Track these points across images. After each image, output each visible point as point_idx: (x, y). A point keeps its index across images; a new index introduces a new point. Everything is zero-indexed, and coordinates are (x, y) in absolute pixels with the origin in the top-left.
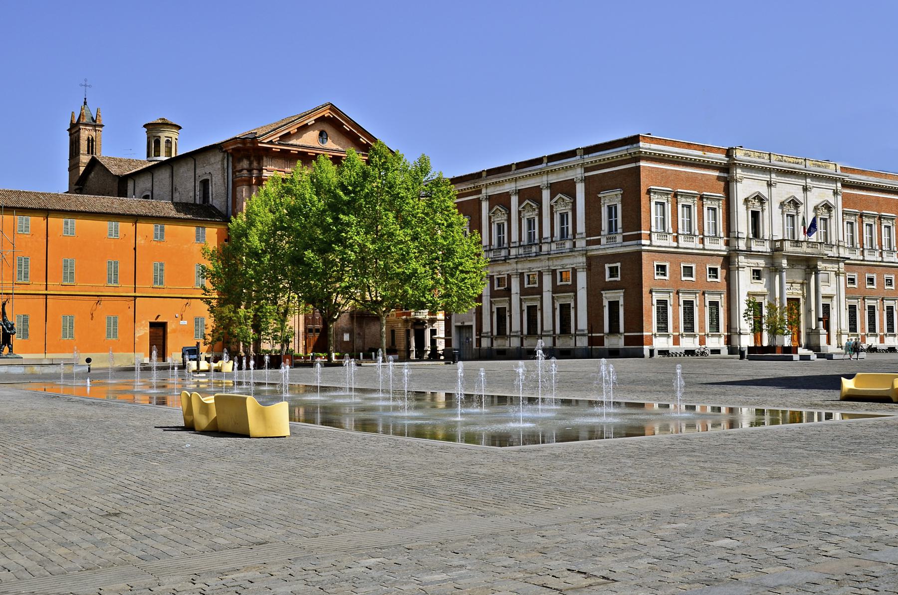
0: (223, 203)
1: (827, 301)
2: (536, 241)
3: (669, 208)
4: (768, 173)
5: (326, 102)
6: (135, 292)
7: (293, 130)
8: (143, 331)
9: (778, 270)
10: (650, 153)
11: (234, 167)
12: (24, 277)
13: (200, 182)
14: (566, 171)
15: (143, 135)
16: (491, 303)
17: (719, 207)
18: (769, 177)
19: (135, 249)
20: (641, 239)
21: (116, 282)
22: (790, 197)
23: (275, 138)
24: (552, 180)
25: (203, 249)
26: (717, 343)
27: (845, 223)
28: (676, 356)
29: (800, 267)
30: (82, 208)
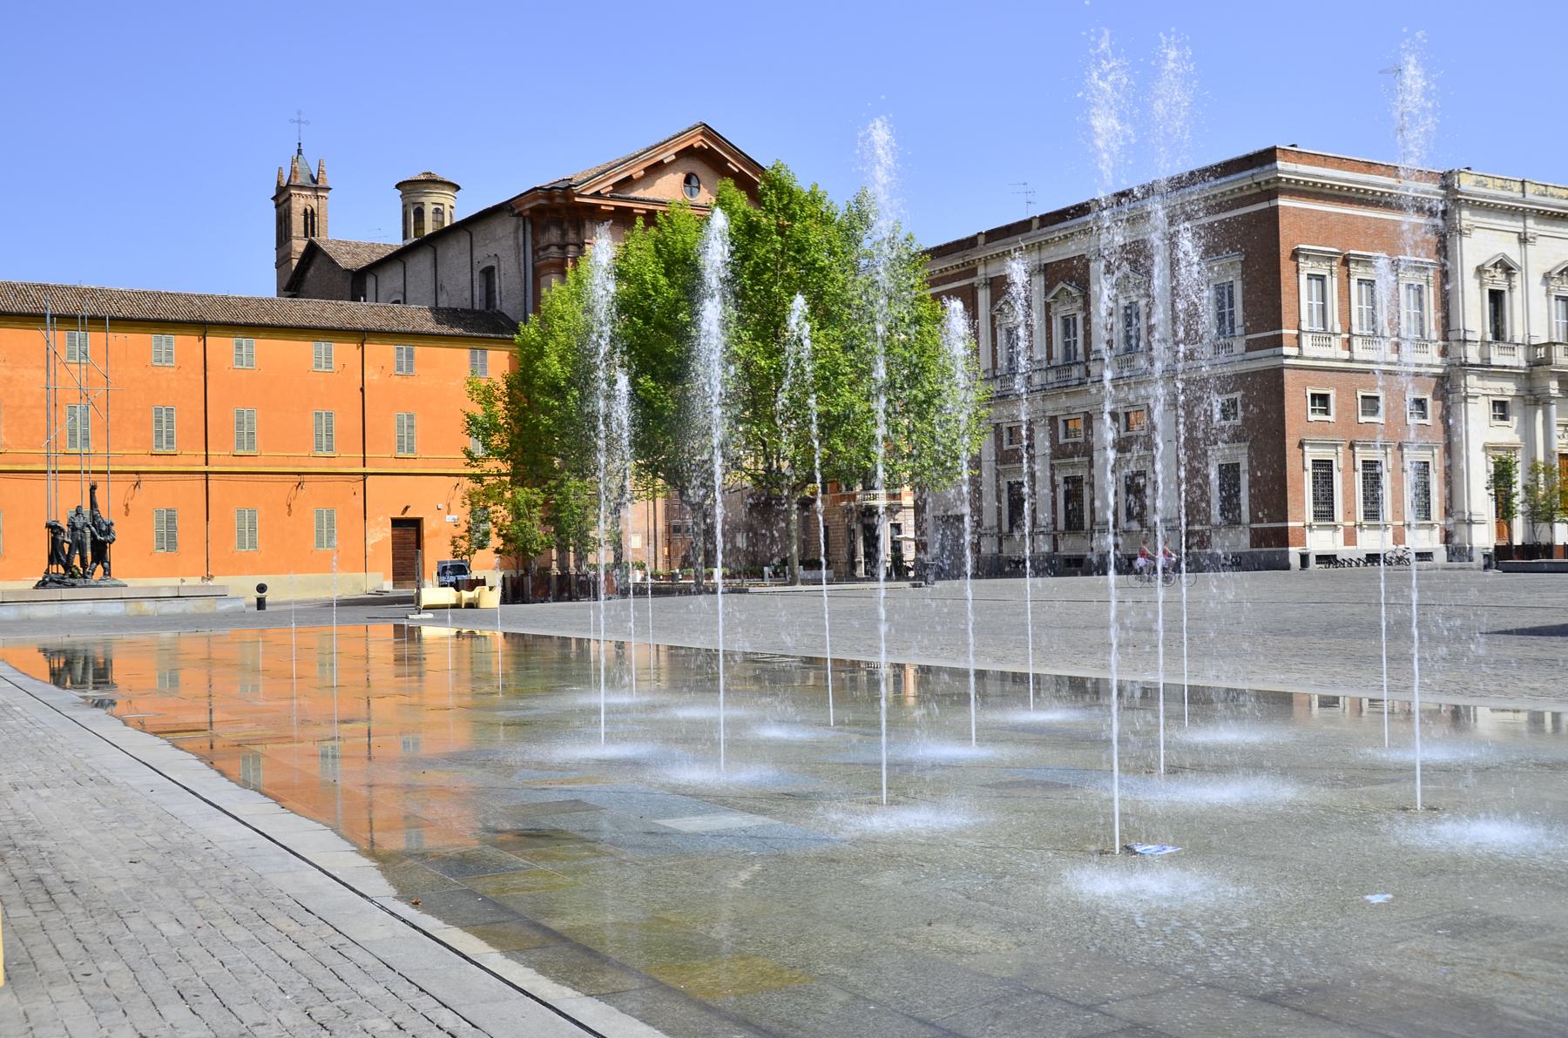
0: (518, 307)
2: (1080, 358)
3: (1333, 285)
4: (1521, 218)
5: (696, 122)
6: (364, 466)
7: (637, 172)
8: (381, 535)
10: (1297, 181)
11: (535, 242)
12: (167, 443)
13: (481, 272)
15: (395, 200)
17: (1428, 283)
19: (362, 390)
20: (1281, 345)
21: (329, 448)
23: (605, 187)
25: (470, 383)
26: (1428, 539)
28: (1350, 565)
30: (267, 320)
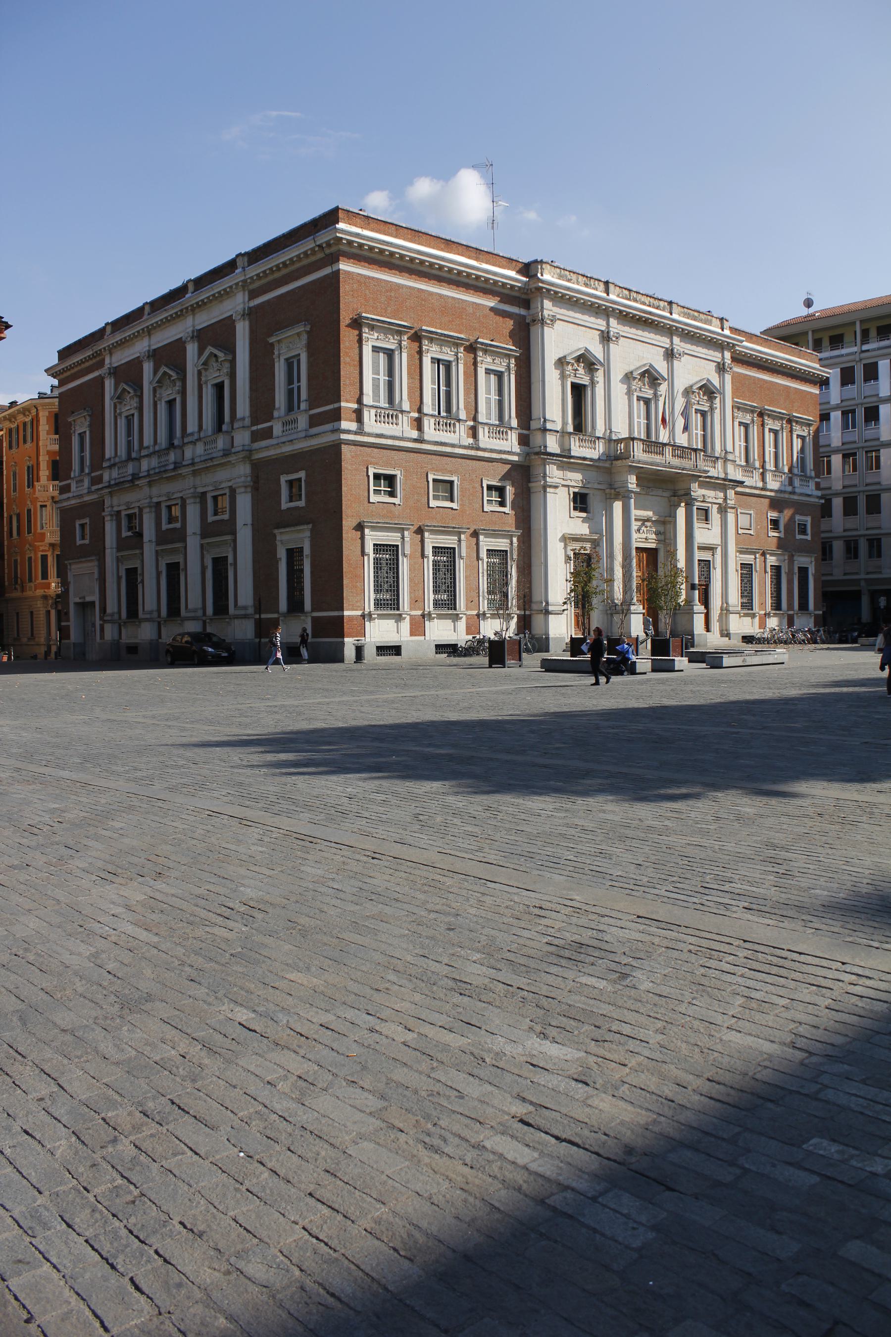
1: (706, 556)
3: (403, 361)
9: (615, 492)
14: (221, 302)
16: (118, 560)
18: (604, 323)
20: (339, 419)
22: (644, 365)
24: (200, 324)
27: (736, 424)
29: (660, 492)
